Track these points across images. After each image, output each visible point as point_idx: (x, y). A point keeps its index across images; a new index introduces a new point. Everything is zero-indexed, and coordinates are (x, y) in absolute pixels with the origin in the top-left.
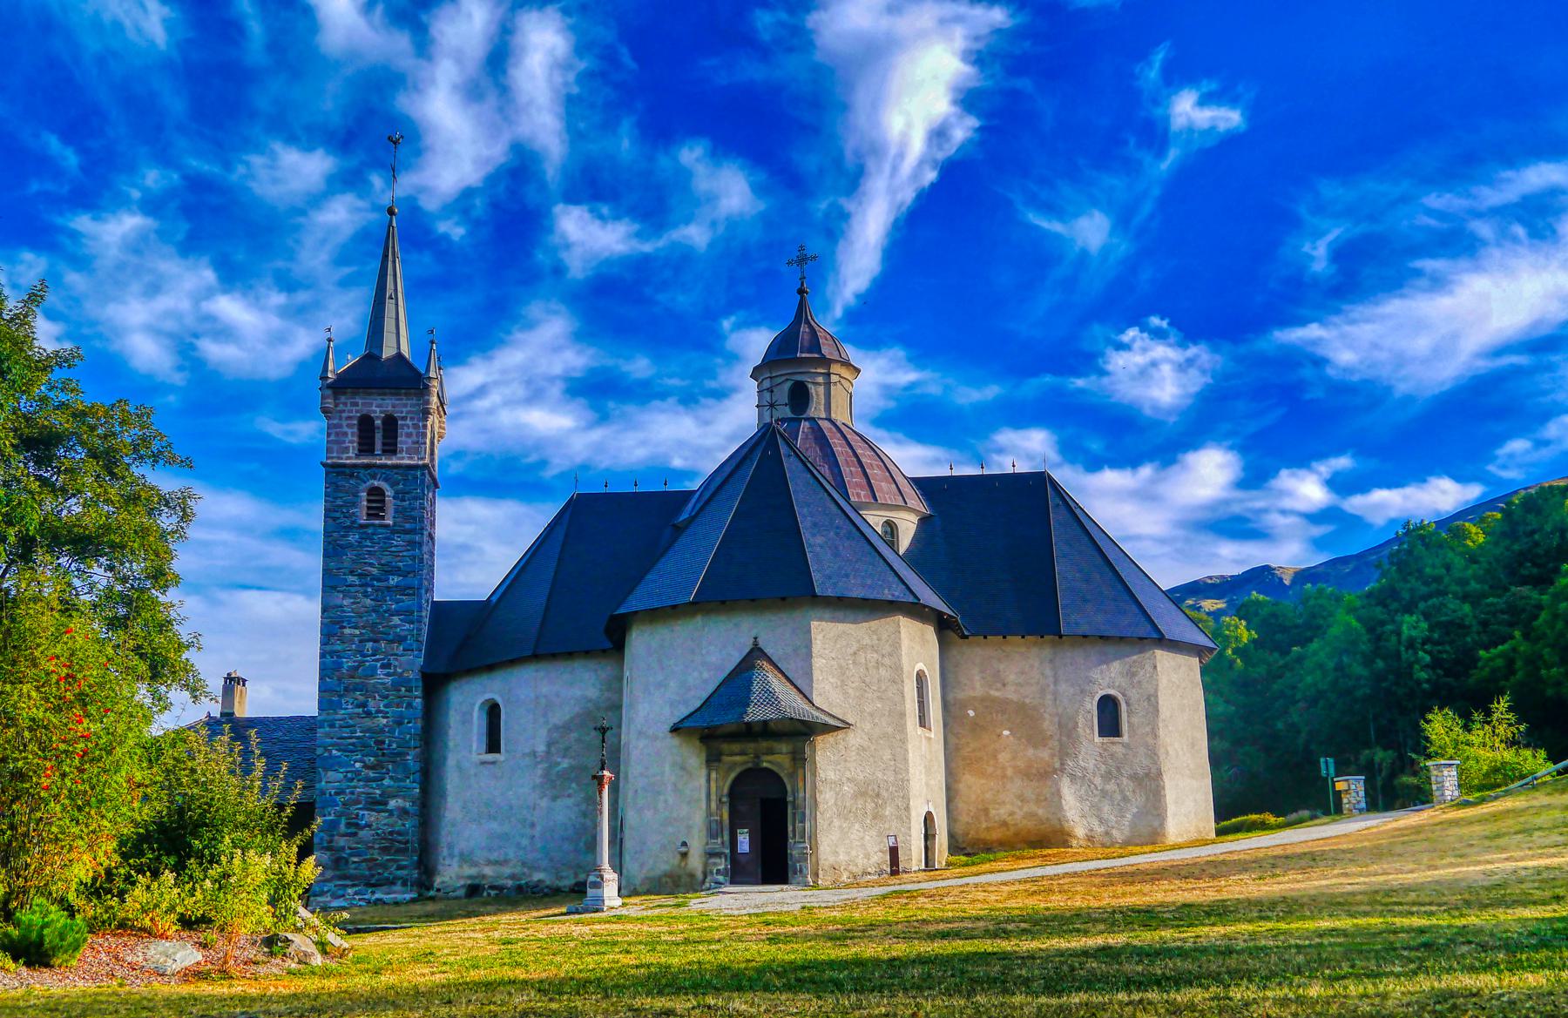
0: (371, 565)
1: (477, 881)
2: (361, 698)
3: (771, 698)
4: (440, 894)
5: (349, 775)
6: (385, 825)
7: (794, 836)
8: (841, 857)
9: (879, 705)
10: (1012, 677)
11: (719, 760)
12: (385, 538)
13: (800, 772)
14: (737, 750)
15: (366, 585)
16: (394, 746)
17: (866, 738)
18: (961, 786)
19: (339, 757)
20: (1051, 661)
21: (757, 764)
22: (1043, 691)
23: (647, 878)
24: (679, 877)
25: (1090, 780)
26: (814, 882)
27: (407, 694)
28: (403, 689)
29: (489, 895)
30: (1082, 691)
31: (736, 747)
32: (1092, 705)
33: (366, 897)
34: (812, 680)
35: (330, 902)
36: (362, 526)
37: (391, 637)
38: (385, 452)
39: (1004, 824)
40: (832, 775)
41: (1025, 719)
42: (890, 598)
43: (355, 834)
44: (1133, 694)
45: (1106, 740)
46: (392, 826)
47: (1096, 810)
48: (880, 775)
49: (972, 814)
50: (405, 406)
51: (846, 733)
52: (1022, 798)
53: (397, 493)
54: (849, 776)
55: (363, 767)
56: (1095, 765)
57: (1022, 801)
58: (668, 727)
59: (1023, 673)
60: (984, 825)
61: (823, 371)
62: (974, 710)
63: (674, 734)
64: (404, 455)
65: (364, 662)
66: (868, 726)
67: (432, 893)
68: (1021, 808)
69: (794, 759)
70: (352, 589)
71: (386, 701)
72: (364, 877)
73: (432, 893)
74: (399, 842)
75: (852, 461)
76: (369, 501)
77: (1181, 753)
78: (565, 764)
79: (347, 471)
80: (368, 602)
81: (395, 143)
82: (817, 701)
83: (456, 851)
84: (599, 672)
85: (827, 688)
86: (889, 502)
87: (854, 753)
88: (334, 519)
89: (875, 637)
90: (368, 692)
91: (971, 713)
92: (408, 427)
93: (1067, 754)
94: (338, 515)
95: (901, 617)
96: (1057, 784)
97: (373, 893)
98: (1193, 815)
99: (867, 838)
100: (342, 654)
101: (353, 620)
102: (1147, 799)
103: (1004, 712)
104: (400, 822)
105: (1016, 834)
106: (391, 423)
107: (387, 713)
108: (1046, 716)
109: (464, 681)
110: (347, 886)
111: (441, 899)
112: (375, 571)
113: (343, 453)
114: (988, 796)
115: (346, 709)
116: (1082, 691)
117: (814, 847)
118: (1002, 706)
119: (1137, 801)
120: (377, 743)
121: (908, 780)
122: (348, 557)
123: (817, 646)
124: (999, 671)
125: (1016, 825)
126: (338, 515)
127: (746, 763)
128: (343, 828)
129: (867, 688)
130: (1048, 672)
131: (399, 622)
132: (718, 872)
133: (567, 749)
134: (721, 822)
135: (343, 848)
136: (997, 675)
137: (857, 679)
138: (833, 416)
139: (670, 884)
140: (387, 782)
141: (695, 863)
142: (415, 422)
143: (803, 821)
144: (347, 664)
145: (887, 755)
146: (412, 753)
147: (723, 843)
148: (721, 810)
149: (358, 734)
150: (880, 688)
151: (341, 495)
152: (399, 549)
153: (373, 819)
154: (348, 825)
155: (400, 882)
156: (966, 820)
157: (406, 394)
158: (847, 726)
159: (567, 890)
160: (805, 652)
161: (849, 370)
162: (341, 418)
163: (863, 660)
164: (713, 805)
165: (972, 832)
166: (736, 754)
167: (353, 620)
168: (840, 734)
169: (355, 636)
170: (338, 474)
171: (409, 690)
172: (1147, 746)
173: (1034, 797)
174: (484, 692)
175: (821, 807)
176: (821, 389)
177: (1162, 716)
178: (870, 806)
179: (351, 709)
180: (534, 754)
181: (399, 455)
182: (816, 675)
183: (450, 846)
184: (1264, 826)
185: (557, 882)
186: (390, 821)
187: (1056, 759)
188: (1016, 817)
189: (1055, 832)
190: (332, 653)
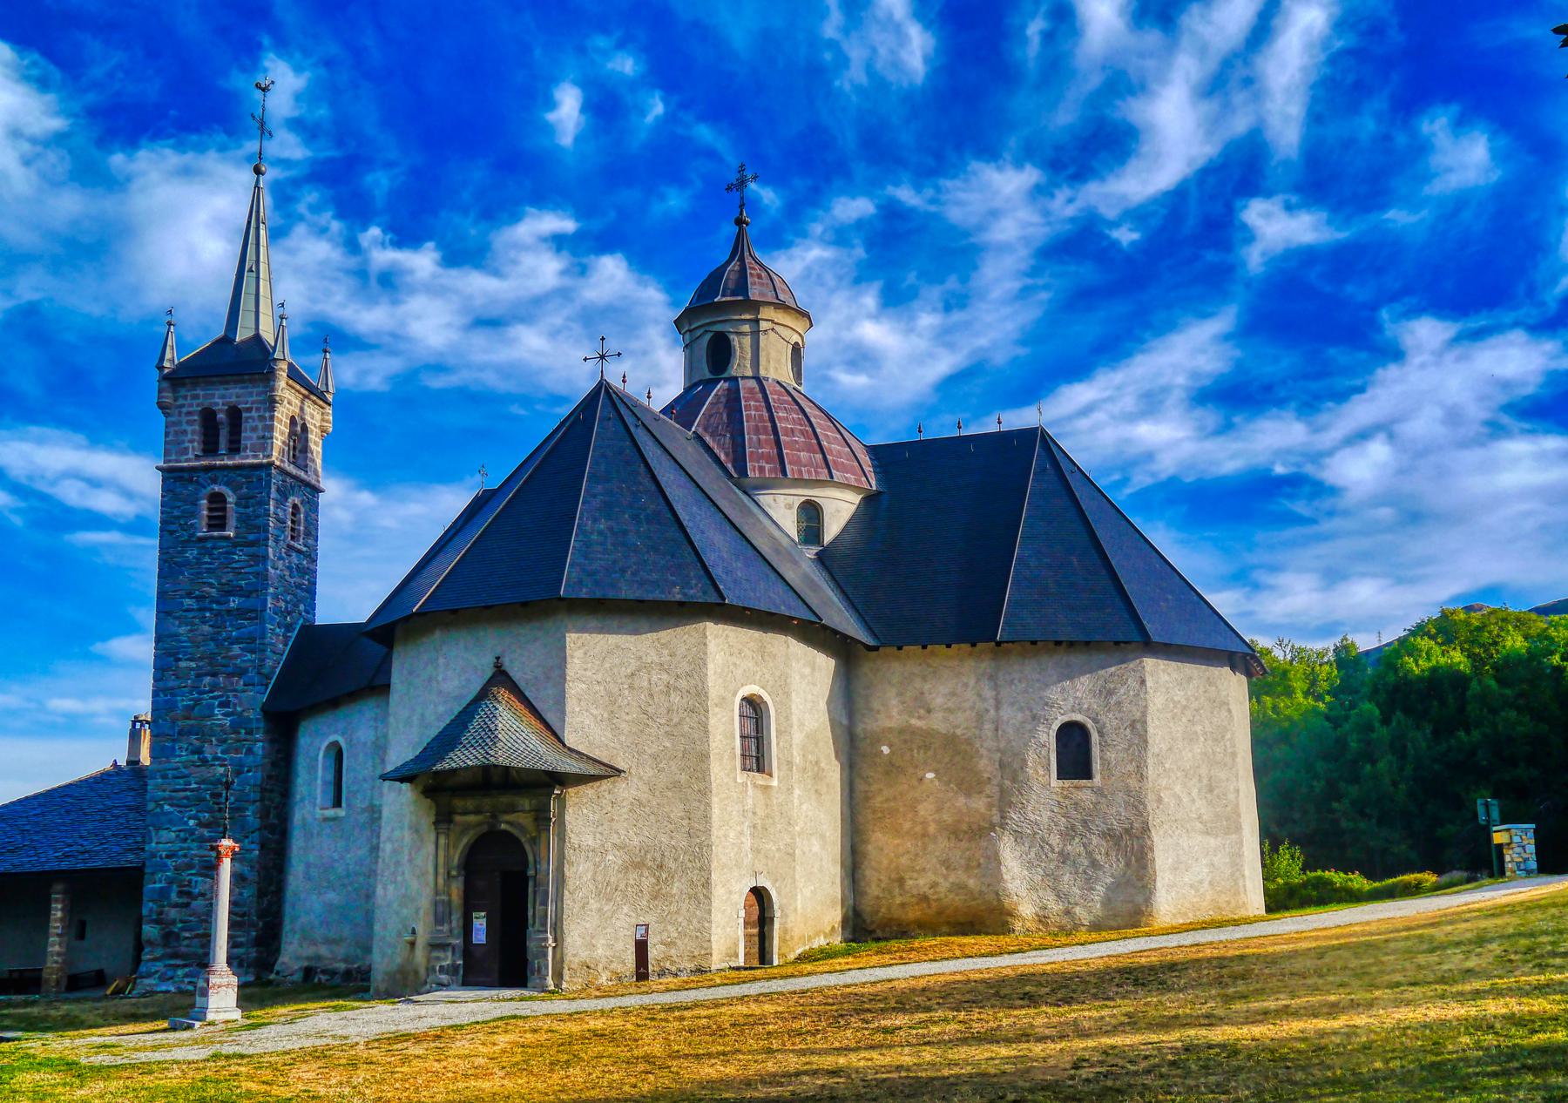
0: (211, 585)
1: (313, 964)
2: (197, 743)
4: (280, 978)
5: (182, 834)
7: (534, 922)
8: (600, 951)
9: (668, 745)
11: (450, 821)
12: (226, 553)
13: (544, 835)
19: (172, 813)
20: (991, 678)
22: (980, 718)
25: (1043, 839)
26: (556, 986)
27: (248, 737)
30: (1034, 717)
31: (470, 804)
32: (1048, 737)
34: (563, 713)
35: (156, 985)
36: (201, 540)
37: (230, 670)
39: (924, 898)
40: (589, 840)
43: (187, 905)
44: (1109, 721)
45: (1067, 783)
47: (1052, 879)
48: (664, 839)
49: (883, 885)
50: (251, 394)
51: (614, 782)
52: (947, 864)
53: (240, 498)
56: (1050, 818)
57: (947, 868)
59: (953, 694)
60: (898, 900)
61: (748, 317)
62: (890, 746)
64: (249, 452)
65: (201, 699)
66: (648, 773)
67: (272, 976)
68: (946, 877)
69: (536, 819)
70: (190, 615)
71: (225, 746)
72: (196, 954)
73: (272, 976)
75: (765, 427)
76: (210, 510)
77: (1185, 800)
79: (186, 475)
80: (206, 628)
81: (263, 90)
82: (570, 739)
87: (625, 810)
89: (666, 652)
90: (204, 734)
91: (886, 750)
98: (1206, 884)
101: (190, 650)
102: (1128, 865)
103: (926, 747)
105: (940, 913)
106: (235, 414)
107: (225, 760)
108: (983, 752)
110: (178, 966)
112: (213, 591)
113: (182, 454)
114: (904, 860)
115: (180, 756)
116: (1034, 717)
118: (926, 739)
119: (1113, 867)
121: (709, 846)
122: (185, 576)
124: (922, 693)
125: (938, 900)
126: (173, 527)
127: (479, 824)
128: (174, 897)
129: (650, 722)
130: (989, 693)
134: (450, 902)
135: (174, 922)
138: (762, 373)
143: (545, 903)
144: (183, 702)
146: (252, 808)
147: (451, 931)
149: (194, 786)
154: (180, 894)
156: (876, 893)
157: (251, 381)
158: (614, 772)
161: (789, 314)
163: (645, 684)
164: (441, 881)
165: (883, 910)
167: (190, 650)
168: (605, 785)
169: (192, 669)
171: (249, 732)
172: (1128, 792)
173: (963, 862)
175: (571, 883)
176: (747, 341)
178: (648, 882)
179: (185, 756)
181: (242, 454)
182: (571, 705)
187: (995, 810)
188: (940, 889)
189: (991, 910)
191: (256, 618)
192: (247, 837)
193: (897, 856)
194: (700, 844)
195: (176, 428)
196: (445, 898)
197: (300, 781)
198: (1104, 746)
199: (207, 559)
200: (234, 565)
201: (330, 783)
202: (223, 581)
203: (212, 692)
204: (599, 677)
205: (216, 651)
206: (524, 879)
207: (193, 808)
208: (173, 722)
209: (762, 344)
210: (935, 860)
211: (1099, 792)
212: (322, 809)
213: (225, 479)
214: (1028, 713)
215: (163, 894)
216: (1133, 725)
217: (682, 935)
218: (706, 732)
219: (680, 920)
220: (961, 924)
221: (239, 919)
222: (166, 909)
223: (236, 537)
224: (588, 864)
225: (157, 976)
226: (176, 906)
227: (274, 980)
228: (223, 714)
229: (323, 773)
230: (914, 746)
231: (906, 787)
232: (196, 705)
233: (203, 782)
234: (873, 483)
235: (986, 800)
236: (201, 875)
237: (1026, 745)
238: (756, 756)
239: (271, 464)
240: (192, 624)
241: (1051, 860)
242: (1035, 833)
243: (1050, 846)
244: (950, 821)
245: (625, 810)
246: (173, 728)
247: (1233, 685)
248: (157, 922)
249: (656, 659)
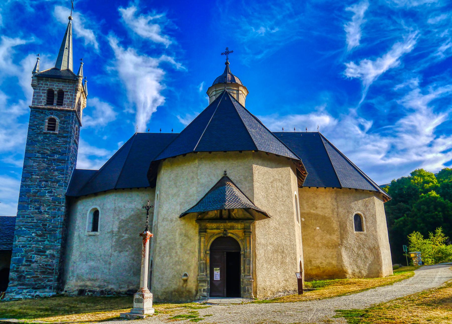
0: (47, 149)
1: (83, 288)
2: (38, 206)
3: (236, 199)
4: (67, 293)
5: (29, 239)
6: (44, 261)
7: (244, 271)
8: (267, 283)
9: (283, 208)
13: (248, 238)
14: (215, 227)
15: (45, 158)
16: (51, 227)
17: (278, 224)
19: (25, 231)
20: (336, 199)
21: (226, 234)
22: (333, 211)
23: (164, 292)
24: (183, 292)
25: (352, 249)
26: (255, 297)
27: (58, 204)
28: (57, 202)
29: (88, 294)
31: (214, 225)
32: (352, 218)
33: (32, 294)
34: (253, 193)
35: (14, 296)
36: (45, 133)
37: (53, 180)
38: (57, 105)
39: (319, 267)
40: (263, 241)
43: (30, 265)
44: (367, 213)
45: (358, 232)
46: (47, 262)
50: (68, 87)
53: (61, 121)
54: (271, 242)
55: (36, 235)
56: (354, 243)
57: (325, 258)
58: (179, 216)
59: (324, 203)
63: (181, 219)
65: (41, 190)
67: (63, 293)
68: (325, 261)
70: (38, 159)
72: (32, 284)
73: (63, 293)
74: (50, 269)
76: (49, 124)
78: (126, 236)
79: (41, 111)
80: (45, 165)
83: (75, 275)
84: (143, 198)
87: (272, 231)
89: (280, 176)
92: (68, 95)
94: (34, 128)
96: (340, 250)
97: (35, 292)
99: (279, 273)
100: (30, 186)
102: (374, 258)
103: (316, 220)
104: (51, 260)
105: (324, 272)
106: (61, 94)
107: (49, 212)
108: (334, 221)
109: (84, 200)
110: (24, 288)
111: (67, 296)
112: (49, 152)
113: (39, 103)
114: (311, 255)
115: (31, 210)
116: (348, 212)
117: (255, 278)
120: (43, 225)
122: (37, 146)
123: (256, 177)
125: (323, 268)
126: (34, 128)
127: (219, 233)
128: (24, 262)
130: (335, 204)
131: (58, 174)
132: (204, 290)
133: (127, 230)
135: (23, 271)
136: (313, 204)
137: (273, 195)
139: (177, 296)
140: (46, 242)
141: (192, 285)
142: (72, 93)
143: (249, 264)
145: (287, 233)
147: (206, 275)
148: (206, 258)
150: (283, 200)
151: (37, 120)
152: (60, 144)
153: (38, 259)
154: (27, 261)
155: (48, 288)
159: (124, 293)
162: (40, 89)
164: (202, 255)
166: (215, 229)
169: (38, 179)
170: (36, 111)
174: (93, 205)
180: (112, 232)
181: (63, 106)
182: (256, 190)
183: (73, 272)
185: (119, 289)
186: (46, 260)
187: (339, 240)
188: (323, 264)
189: (340, 271)
190: (26, 186)
191: (65, 163)
192: (56, 241)
193: (309, 253)
194: (293, 244)
195: (38, 94)
197: (78, 222)
199: (47, 140)
200: (57, 144)
201: (91, 223)
202: (53, 149)
203: (45, 187)
204: (263, 182)
205: (48, 173)
206: (238, 255)
207: (34, 229)
208: (29, 197)
209: (240, 97)
210: (321, 255)
211: (366, 235)
212: (88, 232)
213: (56, 114)
214: (346, 210)
215: (20, 261)
216: (372, 216)
217: (290, 277)
219: (289, 272)
220: (330, 275)
221: (51, 271)
222: (20, 267)
223: (59, 134)
224: (263, 250)
225: (15, 292)
226: (25, 265)
227: (65, 294)
228: (49, 196)
229: (89, 218)
230: (313, 219)
231: (310, 231)
232: (38, 192)
233: (40, 220)
235: (336, 236)
236: (36, 254)
237: (346, 220)
240: (39, 163)
241: (355, 256)
242: (350, 247)
243: (354, 251)
244: (325, 243)
245: (272, 231)
246: (28, 199)
248: (17, 271)
249: (278, 177)
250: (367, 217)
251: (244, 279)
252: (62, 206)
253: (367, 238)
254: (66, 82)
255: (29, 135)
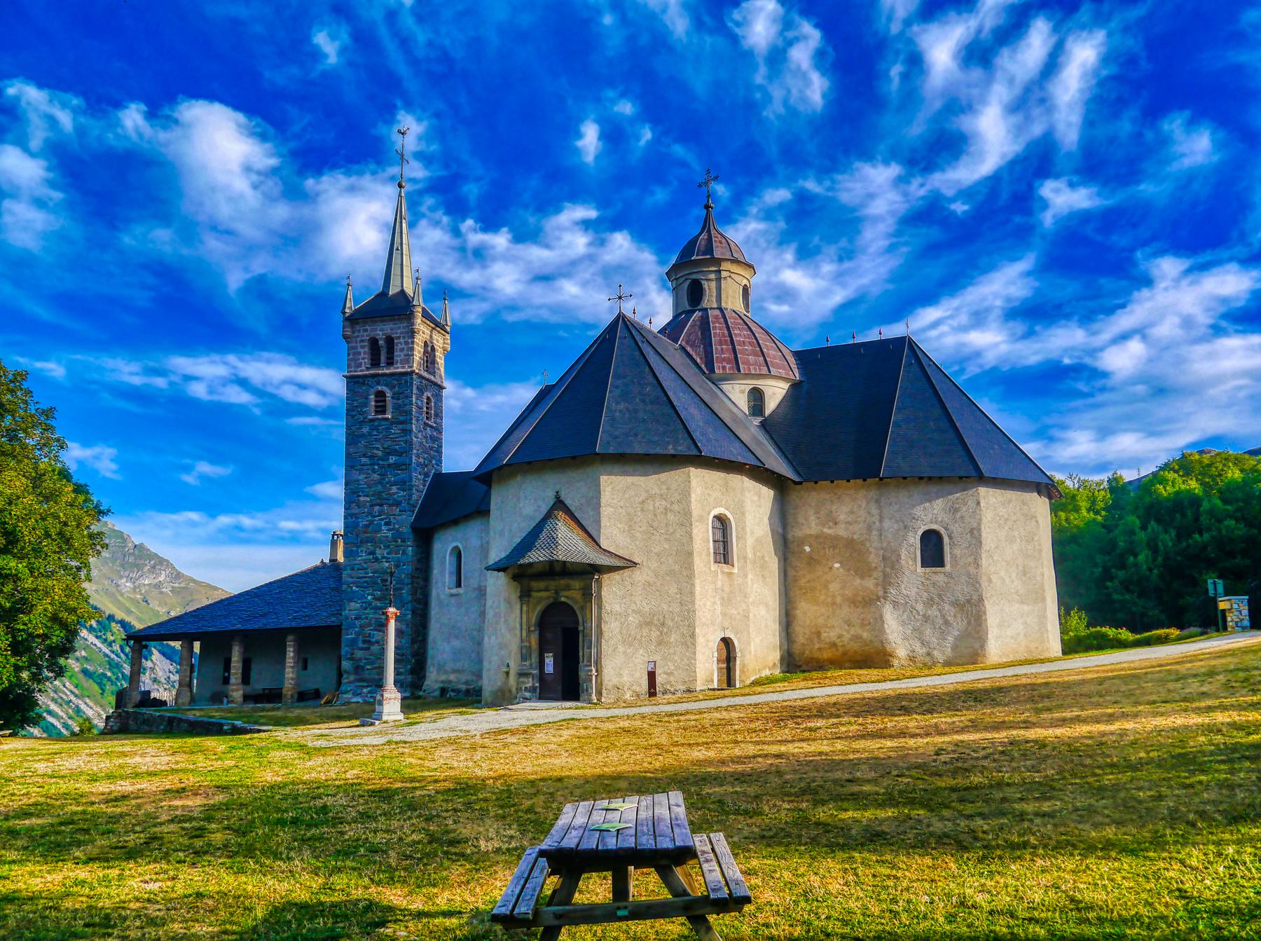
0: (378, 449)
1: (446, 685)
8: (625, 678)
10: (842, 517)
11: (529, 596)
13: (588, 605)
18: (798, 613)
20: (877, 501)
22: (869, 528)
30: (905, 527)
31: (542, 585)
32: (915, 540)
34: (600, 526)
37: (391, 502)
39: (834, 645)
40: (617, 608)
41: (853, 552)
42: (672, 452)
43: (369, 649)
44: (956, 529)
45: (928, 570)
47: (918, 633)
48: (665, 607)
52: (849, 623)
59: (852, 512)
60: (817, 646)
61: (714, 269)
66: (654, 565)
67: (421, 693)
68: (848, 632)
70: (365, 468)
76: (376, 401)
79: (361, 380)
80: (376, 476)
82: (604, 544)
85: (615, 532)
86: (753, 372)
88: (353, 416)
89: (664, 487)
91: (807, 549)
93: (890, 584)
94: (354, 413)
95: (692, 469)
98: (1022, 636)
102: (969, 623)
103: (834, 547)
105: (844, 654)
106: (390, 341)
108: (872, 550)
112: (380, 453)
114: (821, 621)
116: (905, 527)
118: (834, 542)
121: (694, 611)
123: (606, 497)
126: (354, 413)
127: (548, 598)
128: (360, 645)
129: (654, 532)
130: (875, 511)
134: (530, 647)
135: (361, 659)
138: (723, 305)
143: (590, 648)
144: (363, 522)
145: (673, 590)
154: (364, 642)
157: (399, 319)
160: (595, 502)
163: (651, 508)
168: (627, 572)
171: (404, 541)
172: (969, 575)
175: (606, 635)
176: (713, 284)
177: (985, 547)
178: (655, 634)
182: (604, 522)
184: (1123, 645)
187: (880, 588)
189: (878, 653)
190: (352, 515)
196: (527, 644)
198: (952, 545)
208: (357, 535)
211: (949, 575)
215: (354, 641)
217: (677, 668)
218: (691, 538)
220: (858, 661)
226: (362, 649)
229: (449, 562)
231: (821, 573)
234: (797, 375)
238: (724, 554)
239: (413, 372)
247: (1040, 506)
248: (352, 659)
250: (955, 535)
251: (587, 671)
252: (408, 546)
253: (952, 581)
254: (395, 320)
255: (348, 427)
